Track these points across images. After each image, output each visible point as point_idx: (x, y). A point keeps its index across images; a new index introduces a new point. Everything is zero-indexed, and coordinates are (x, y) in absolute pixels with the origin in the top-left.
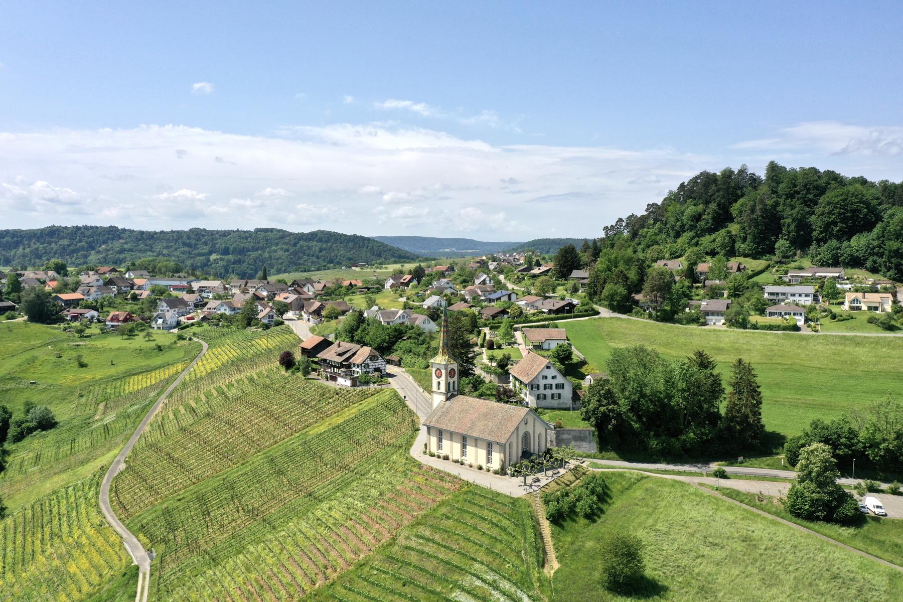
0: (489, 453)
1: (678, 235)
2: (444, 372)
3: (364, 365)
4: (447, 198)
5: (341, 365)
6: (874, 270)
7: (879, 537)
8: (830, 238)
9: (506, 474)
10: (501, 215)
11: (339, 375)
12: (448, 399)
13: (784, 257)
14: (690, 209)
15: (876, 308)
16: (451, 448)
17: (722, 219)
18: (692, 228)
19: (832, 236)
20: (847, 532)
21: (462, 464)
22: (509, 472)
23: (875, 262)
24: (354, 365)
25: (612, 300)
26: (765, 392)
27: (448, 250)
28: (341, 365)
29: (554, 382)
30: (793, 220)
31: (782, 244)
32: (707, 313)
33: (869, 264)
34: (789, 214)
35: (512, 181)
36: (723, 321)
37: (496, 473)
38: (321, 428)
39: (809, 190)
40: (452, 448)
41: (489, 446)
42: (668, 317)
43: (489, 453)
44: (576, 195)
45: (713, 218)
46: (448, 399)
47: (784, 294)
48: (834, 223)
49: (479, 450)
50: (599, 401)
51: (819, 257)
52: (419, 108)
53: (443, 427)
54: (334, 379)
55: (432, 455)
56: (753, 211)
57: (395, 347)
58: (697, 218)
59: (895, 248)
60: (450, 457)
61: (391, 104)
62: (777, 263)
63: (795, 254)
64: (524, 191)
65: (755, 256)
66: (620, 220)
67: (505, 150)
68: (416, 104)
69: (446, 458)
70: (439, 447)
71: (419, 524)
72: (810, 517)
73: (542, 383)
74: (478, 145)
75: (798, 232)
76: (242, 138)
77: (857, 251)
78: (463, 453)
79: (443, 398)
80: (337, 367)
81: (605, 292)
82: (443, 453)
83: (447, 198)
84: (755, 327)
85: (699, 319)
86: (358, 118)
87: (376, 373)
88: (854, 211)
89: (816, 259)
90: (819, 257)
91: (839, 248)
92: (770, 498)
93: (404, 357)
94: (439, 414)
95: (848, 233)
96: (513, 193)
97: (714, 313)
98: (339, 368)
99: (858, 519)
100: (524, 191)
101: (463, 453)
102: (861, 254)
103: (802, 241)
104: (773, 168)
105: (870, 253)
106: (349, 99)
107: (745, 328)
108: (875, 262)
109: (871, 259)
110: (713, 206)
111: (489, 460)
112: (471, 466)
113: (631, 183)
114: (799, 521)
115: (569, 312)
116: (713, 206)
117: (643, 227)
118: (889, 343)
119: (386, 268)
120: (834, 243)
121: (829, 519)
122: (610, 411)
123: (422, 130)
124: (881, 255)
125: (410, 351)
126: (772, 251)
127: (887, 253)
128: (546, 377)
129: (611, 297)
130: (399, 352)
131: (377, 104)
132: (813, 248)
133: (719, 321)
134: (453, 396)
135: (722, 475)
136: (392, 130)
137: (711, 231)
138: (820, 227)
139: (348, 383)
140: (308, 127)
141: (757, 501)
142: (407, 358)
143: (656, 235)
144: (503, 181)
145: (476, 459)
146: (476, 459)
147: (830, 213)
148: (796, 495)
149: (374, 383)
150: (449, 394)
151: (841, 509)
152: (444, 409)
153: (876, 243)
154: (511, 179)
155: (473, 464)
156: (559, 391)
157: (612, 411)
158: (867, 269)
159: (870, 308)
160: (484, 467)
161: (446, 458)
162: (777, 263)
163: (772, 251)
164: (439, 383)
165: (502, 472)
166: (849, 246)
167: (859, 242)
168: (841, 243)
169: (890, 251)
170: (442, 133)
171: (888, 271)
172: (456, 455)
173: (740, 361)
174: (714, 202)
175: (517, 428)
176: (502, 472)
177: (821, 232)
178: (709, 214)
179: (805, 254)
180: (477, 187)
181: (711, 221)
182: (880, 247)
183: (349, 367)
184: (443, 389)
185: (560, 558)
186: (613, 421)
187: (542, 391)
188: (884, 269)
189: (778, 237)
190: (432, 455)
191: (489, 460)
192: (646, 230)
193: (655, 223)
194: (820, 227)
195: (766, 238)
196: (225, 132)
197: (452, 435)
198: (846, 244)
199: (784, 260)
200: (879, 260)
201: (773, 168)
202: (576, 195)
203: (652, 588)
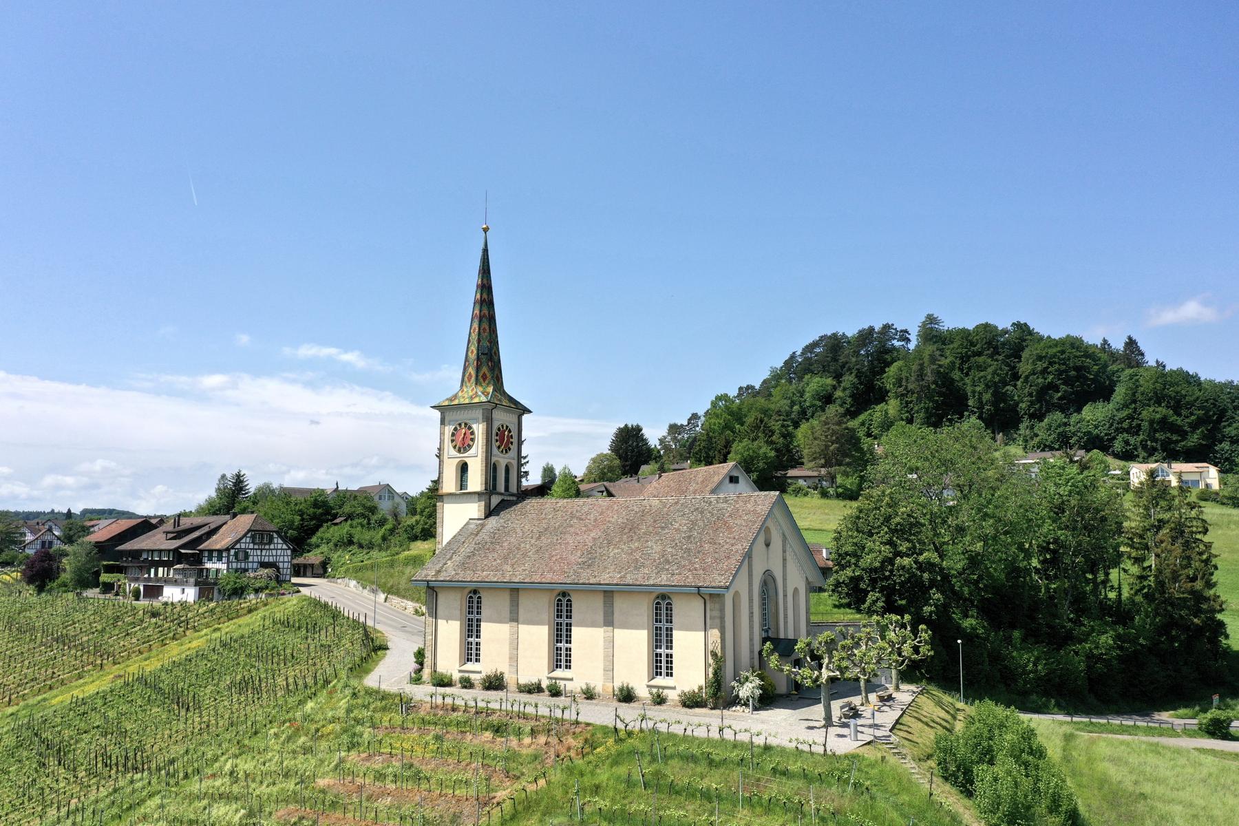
0: (661, 637)
2: (479, 429)
3: (234, 552)
5: (178, 556)
8: (1048, 411)
9: (734, 701)
11: (168, 582)
12: (490, 513)
14: (816, 384)
19: (1051, 407)
21: (555, 692)
22: (745, 691)
23: (1127, 443)
28: (178, 556)
30: (988, 386)
33: (1118, 445)
34: (974, 387)
37: (691, 702)
40: (515, 645)
43: (661, 637)
46: (490, 513)
48: (1053, 387)
50: (890, 543)
51: (1036, 440)
52: (350, 357)
53: (484, 574)
54: (153, 591)
56: (921, 376)
57: (314, 540)
60: (509, 678)
61: (307, 351)
66: (695, 416)
68: (346, 352)
69: (495, 683)
70: (471, 652)
75: (995, 404)
76: (71, 388)
77: (1096, 427)
78: (561, 658)
79: (474, 510)
86: (262, 367)
87: (265, 572)
88: (1077, 369)
89: (1032, 443)
90: (1036, 440)
91: (1065, 424)
93: (334, 557)
94: (465, 550)
95: (1077, 402)
98: (168, 564)
101: (561, 658)
102: (1102, 432)
105: (1117, 429)
106: (244, 339)
108: (1127, 443)
109: (1120, 438)
110: (849, 379)
111: (661, 664)
116: (849, 379)
120: (1058, 416)
122: (920, 567)
123: (357, 388)
125: (351, 543)
127: (1145, 425)
130: (324, 548)
131: (287, 351)
132: (1023, 428)
134: (503, 506)
136: (311, 385)
138: (1030, 395)
139: (191, 594)
140: (183, 379)
142: (344, 557)
145: (610, 669)
146: (610, 669)
147: (1044, 371)
149: (257, 591)
150: (495, 500)
152: (484, 535)
153: (1125, 413)
155: (598, 685)
157: (930, 566)
158: (1116, 456)
160: (642, 691)
164: (464, 468)
165: (719, 694)
167: (1093, 414)
168: (1068, 416)
169: (1152, 422)
170: (388, 393)
172: (535, 667)
175: (748, 555)
176: (719, 694)
177: (1032, 403)
178: (844, 389)
179: (1010, 440)
181: (849, 400)
183: (197, 560)
184: (476, 481)
186: (936, 595)
191: (661, 664)
194: (1030, 395)
196: (43, 377)
198: (1075, 418)
200: (1132, 440)
201: (931, 333)
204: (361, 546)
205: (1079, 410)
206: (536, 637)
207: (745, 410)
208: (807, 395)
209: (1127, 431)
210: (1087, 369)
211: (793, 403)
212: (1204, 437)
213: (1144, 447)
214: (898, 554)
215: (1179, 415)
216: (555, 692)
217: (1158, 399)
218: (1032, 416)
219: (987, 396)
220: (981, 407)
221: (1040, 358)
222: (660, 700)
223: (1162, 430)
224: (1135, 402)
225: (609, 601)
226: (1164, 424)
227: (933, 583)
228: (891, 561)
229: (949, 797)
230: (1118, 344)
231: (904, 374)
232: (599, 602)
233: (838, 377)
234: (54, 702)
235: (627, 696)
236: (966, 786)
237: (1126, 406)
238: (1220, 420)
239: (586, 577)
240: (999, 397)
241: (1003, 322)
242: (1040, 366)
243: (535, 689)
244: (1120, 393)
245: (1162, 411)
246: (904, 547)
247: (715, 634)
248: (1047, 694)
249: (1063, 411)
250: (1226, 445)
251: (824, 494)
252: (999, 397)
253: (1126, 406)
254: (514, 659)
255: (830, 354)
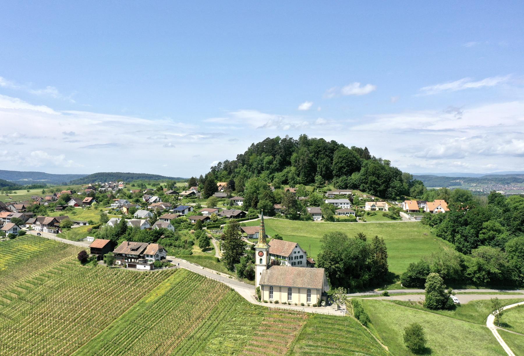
0: (309, 295)
1: (259, 172)
4: (22, 144)
5: (139, 257)
6: (363, 191)
7: (464, 313)
10: (62, 157)
11: (138, 263)
13: (321, 184)
15: (382, 209)
16: (281, 296)
17: (285, 163)
18: (268, 169)
20: (452, 313)
21: (289, 304)
23: (364, 187)
24: (148, 256)
25: (264, 209)
26: (389, 253)
27: (26, 180)
29: (299, 255)
30: (324, 165)
31: (318, 178)
32: (313, 215)
33: (361, 187)
34: (321, 163)
35: (72, 134)
36: (321, 218)
37: (315, 306)
38: (152, 297)
39: (326, 150)
41: (309, 292)
42: (295, 218)
43: (309, 295)
44: (114, 145)
45: (279, 163)
47: (337, 203)
48: (343, 167)
49: (301, 295)
51: (338, 184)
55: (266, 302)
58: (270, 163)
59: (373, 180)
62: (318, 187)
63: (325, 183)
64: (79, 141)
65: (306, 183)
66: (220, 163)
67: (64, 114)
69: (277, 302)
71: (299, 339)
72: (436, 309)
73: (294, 255)
74: (43, 109)
75: (326, 171)
79: (265, 268)
80: (134, 258)
81: (259, 205)
82: (274, 299)
83: (22, 144)
84: (338, 220)
85: (309, 218)
88: (351, 161)
90: (338, 184)
91: (347, 180)
92: (415, 302)
95: (350, 173)
96: (70, 142)
97: (317, 214)
98: (137, 259)
99: (453, 307)
100: (79, 141)
103: (328, 176)
104: (304, 138)
107: (334, 221)
108: (364, 187)
109: (362, 185)
110: (278, 157)
112: (296, 305)
113: (148, 138)
114: (432, 311)
115: (242, 217)
116: (278, 157)
117: (237, 167)
118: (393, 226)
119: (15, 193)
121: (443, 308)
122: (336, 267)
124: (366, 183)
126: (313, 181)
127: (369, 182)
128: (295, 253)
129: (264, 207)
132: (334, 180)
133: (319, 218)
135: (386, 295)
137: (280, 170)
141: (410, 305)
143: (245, 172)
144: (65, 133)
145: (299, 300)
146: (299, 300)
147: (341, 162)
148: (429, 299)
149: (166, 266)
151: (448, 302)
153: (363, 177)
154: (71, 132)
155: (297, 303)
156: (301, 260)
157: (338, 267)
158: (360, 190)
159: (379, 209)
160: (305, 304)
161: (277, 302)
162: (318, 187)
163: (313, 181)
164: (261, 260)
165: (319, 304)
166: (351, 179)
167: (355, 177)
169: (371, 181)
170: (16, 99)
171: (370, 191)
173: (377, 237)
174: (276, 155)
176: (319, 304)
177: (337, 172)
179: (330, 183)
180: (46, 137)
181: (278, 165)
182: (365, 179)
184: (264, 262)
185: (487, 330)
187: (294, 260)
188: (368, 190)
189: (315, 174)
190: (266, 302)
192: (238, 169)
193: (243, 166)
195: (310, 175)
197: (280, 289)
198: (349, 178)
199: (321, 186)
200: (365, 186)
202: (114, 145)
203: (428, 351)
204: (175, 246)
205: (350, 175)
206: (285, 295)
207: (259, 186)
208: (264, 163)
209: (364, 183)
210: (353, 161)
211: (258, 164)
212: (385, 187)
213: (368, 188)
214: (331, 265)
215: (379, 179)
216: (289, 304)
217: (374, 174)
218: (337, 176)
219: (324, 169)
220: (322, 171)
221: (340, 157)
222: (309, 305)
223: (374, 184)
224: (367, 174)
225: (299, 290)
226: (374, 182)
227: (338, 271)
228: (330, 267)
229: (356, 320)
230: (364, 148)
231: (298, 159)
232: (297, 290)
233: (274, 155)
234: (147, 301)
235: (303, 305)
236: (358, 318)
237: (364, 175)
238: (389, 181)
239: (295, 286)
240: (328, 168)
241: (328, 139)
242: (340, 160)
243: (285, 303)
244: (363, 170)
245: (374, 178)
246: (333, 263)
247: (318, 296)
248: (356, 289)
249: (346, 175)
250: (390, 189)
251: (287, 217)
252: (328, 168)
253: (364, 175)
254: (280, 298)
255: (270, 146)
